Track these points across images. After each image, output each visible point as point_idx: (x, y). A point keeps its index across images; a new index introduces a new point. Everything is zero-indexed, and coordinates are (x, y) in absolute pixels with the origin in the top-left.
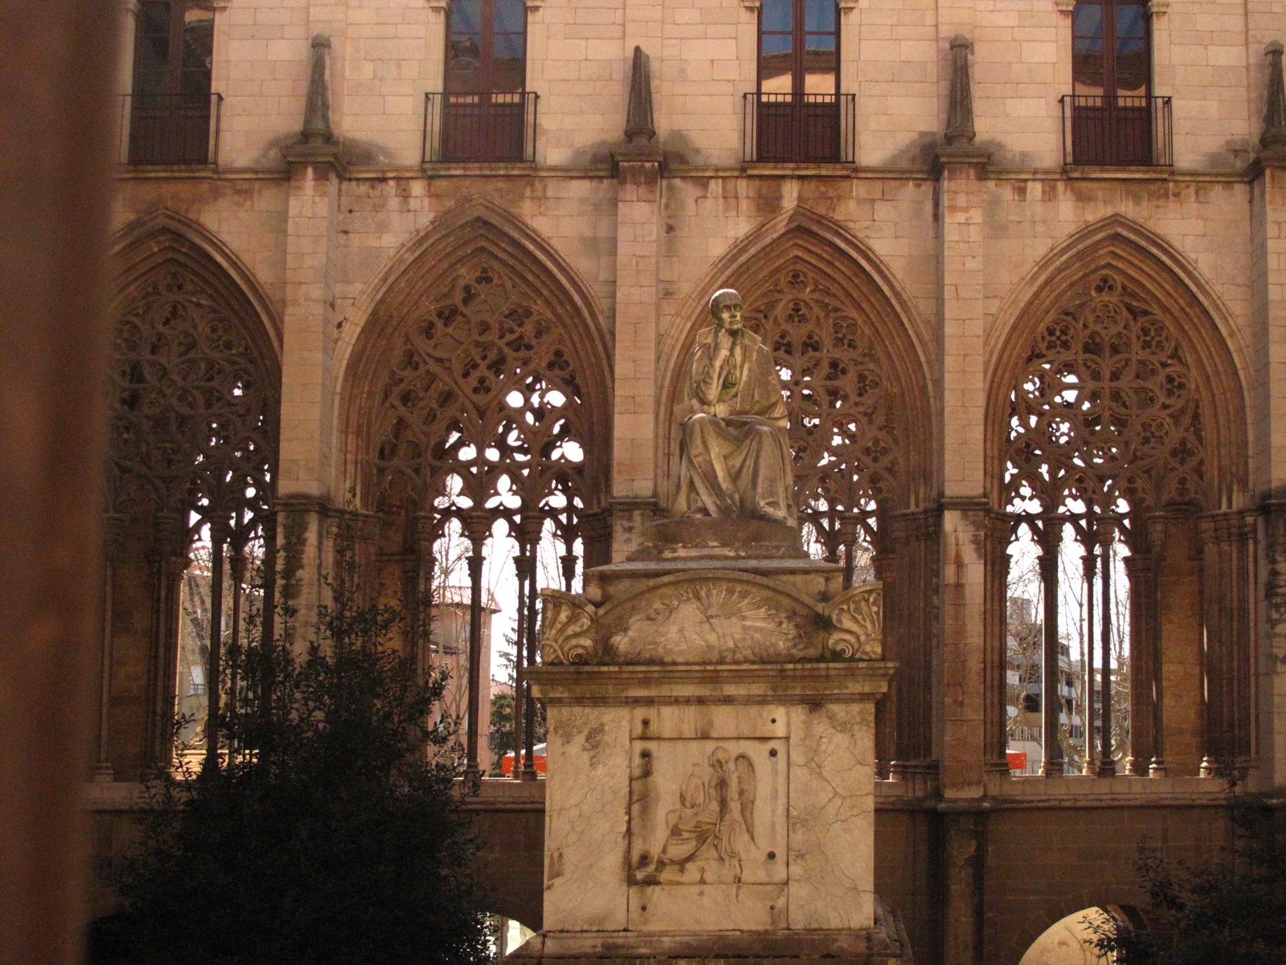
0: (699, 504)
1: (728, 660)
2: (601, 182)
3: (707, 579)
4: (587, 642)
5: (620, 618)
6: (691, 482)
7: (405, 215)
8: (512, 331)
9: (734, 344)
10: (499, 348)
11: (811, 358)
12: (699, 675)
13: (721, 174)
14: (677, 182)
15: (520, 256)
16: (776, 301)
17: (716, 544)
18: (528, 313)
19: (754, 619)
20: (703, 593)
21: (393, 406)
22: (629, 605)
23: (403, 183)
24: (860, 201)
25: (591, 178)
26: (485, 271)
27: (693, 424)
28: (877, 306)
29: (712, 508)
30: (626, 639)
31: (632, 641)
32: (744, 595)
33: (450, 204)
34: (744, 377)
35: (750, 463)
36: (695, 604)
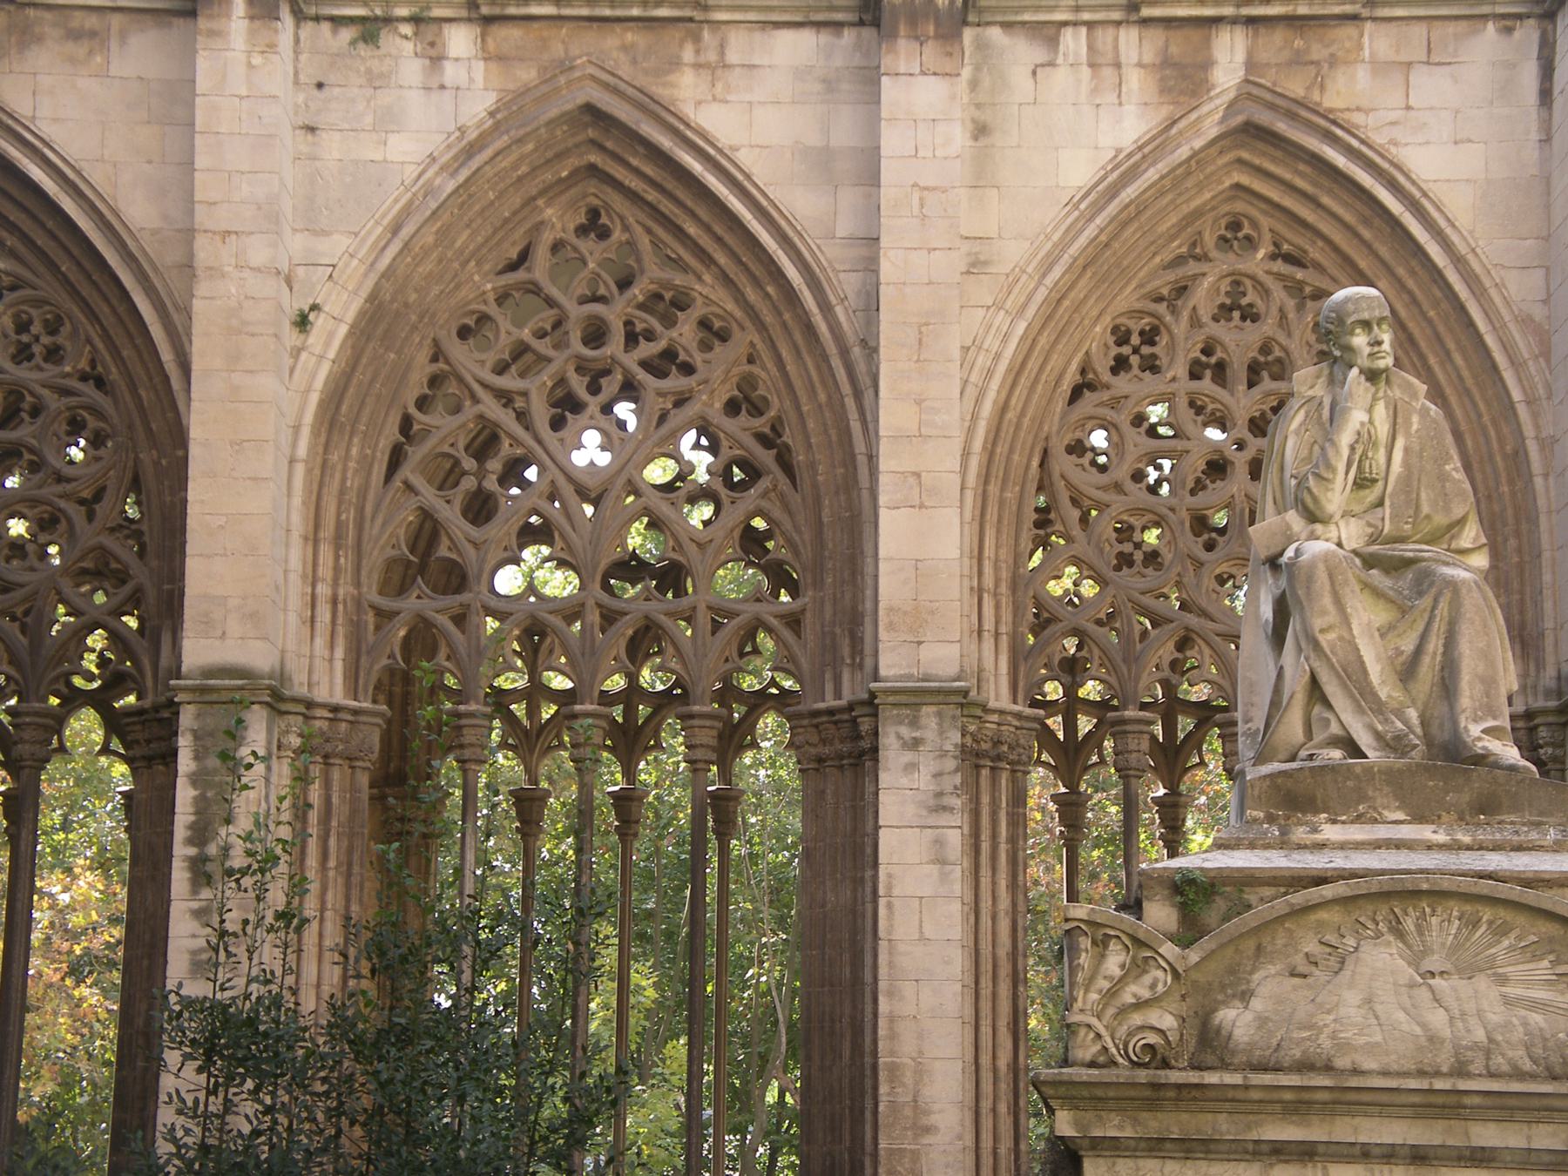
0: (1335, 729)
1: (1473, 1068)
2: (839, 35)
3: (1416, 894)
4: (1168, 1022)
5: (1232, 971)
6: (1314, 682)
7: (435, 96)
8: (650, 336)
9: (1375, 399)
10: (626, 372)
11: (1268, 394)
12: (1416, 1099)
13: (1086, 16)
14: (995, 33)
15: (670, 185)
16: (1195, 277)
17: (1400, 816)
18: (681, 303)
19: (1528, 983)
20: (1409, 924)
21: (409, 487)
22: (1250, 945)
23: (429, 31)
24: (1380, 67)
25: (818, 25)
26: (594, 214)
27: (1312, 565)
28: (1411, 283)
29: (1364, 740)
30: (1248, 1016)
31: (1262, 1021)
32: (1501, 931)
33: (527, 74)
34: (1397, 466)
35: (1435, 644)
36: (1396, 946)
